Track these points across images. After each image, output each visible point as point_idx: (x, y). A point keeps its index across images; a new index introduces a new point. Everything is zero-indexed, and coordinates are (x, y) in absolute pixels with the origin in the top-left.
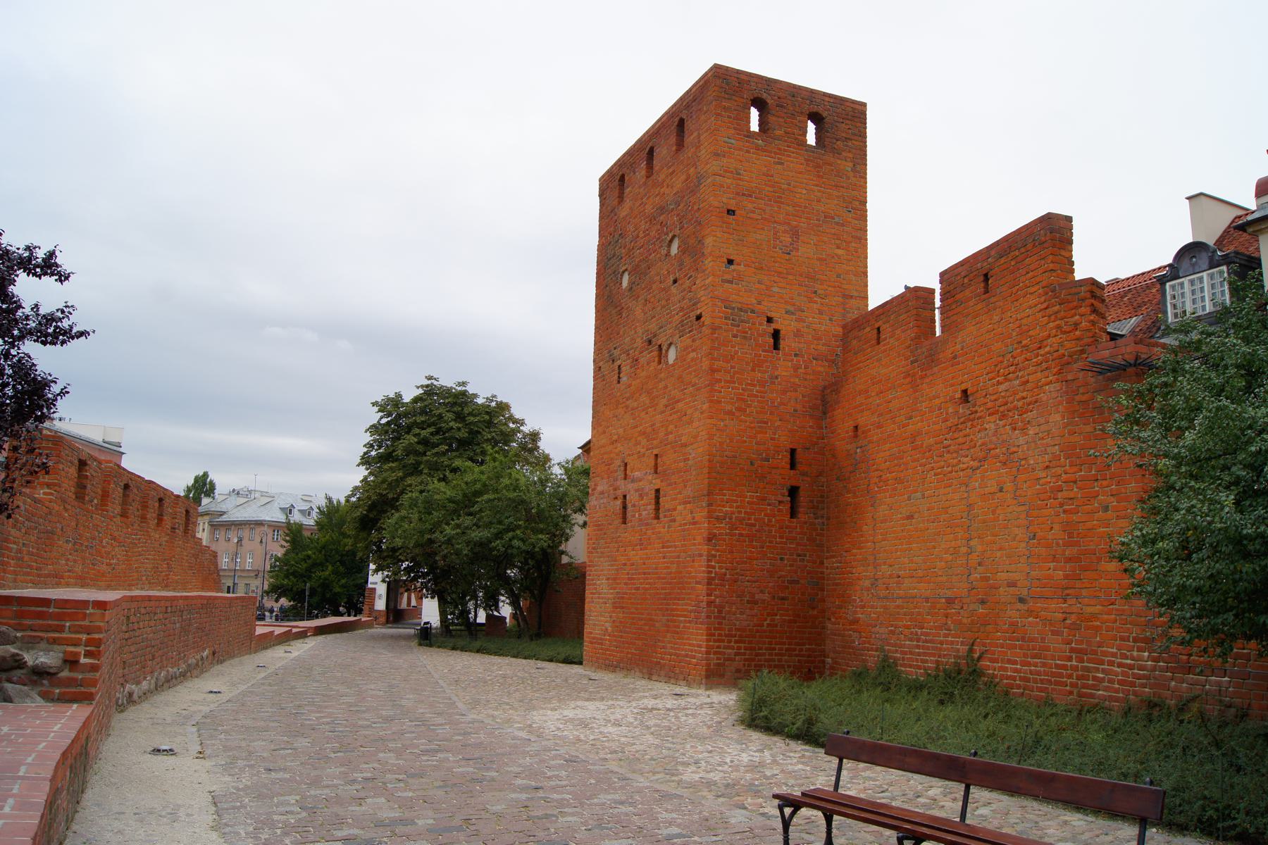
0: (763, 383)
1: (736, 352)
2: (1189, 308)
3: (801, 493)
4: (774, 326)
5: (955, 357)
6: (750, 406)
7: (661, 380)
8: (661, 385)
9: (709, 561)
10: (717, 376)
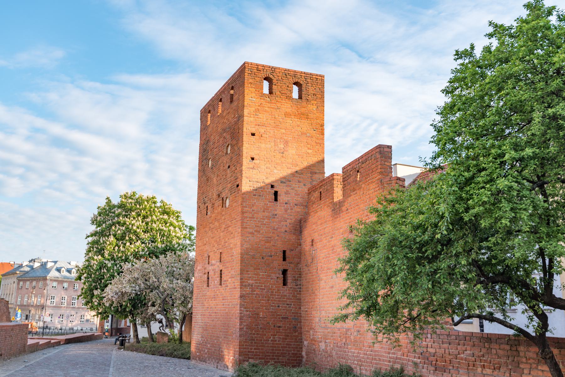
0: (268, 218)
1: (255, 203)
2: (35, 302)
3: (288, 272)
4: (275, 189)
5: (347, 210)
6: (262, 230)
7: (223, 215)
8: (223, 218)
9: (240, 307)
10: (245, 215)
